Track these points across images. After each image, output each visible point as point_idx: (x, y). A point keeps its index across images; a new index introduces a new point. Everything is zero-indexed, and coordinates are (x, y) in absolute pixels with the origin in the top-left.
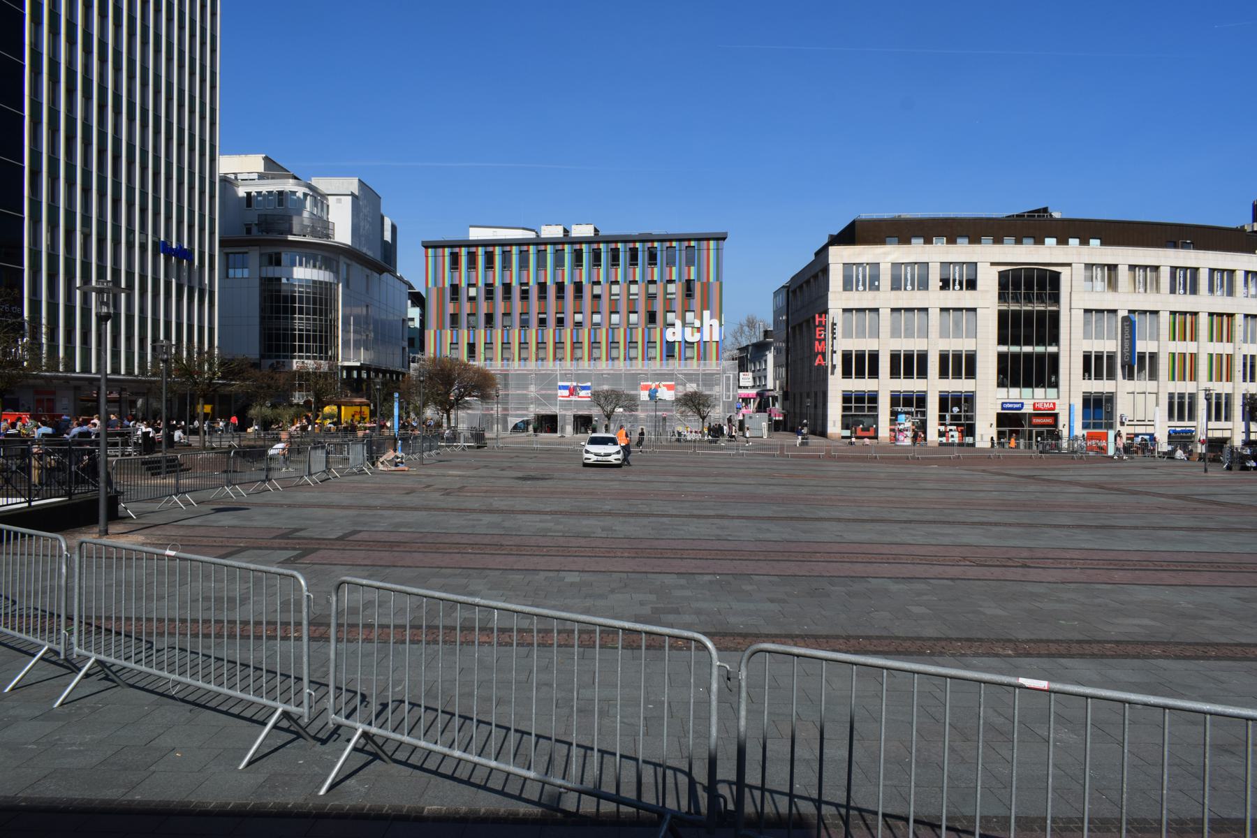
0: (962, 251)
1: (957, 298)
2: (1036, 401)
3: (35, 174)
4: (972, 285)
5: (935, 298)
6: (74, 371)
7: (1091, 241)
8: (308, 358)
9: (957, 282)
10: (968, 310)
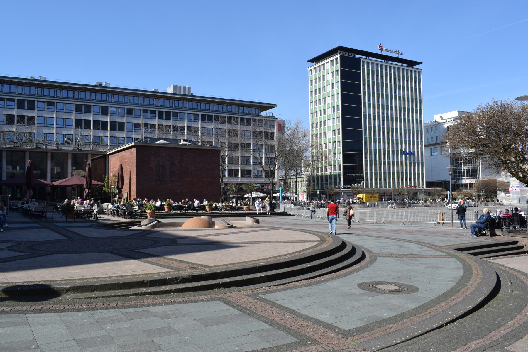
3: (366, 142)
6: (378, 188)
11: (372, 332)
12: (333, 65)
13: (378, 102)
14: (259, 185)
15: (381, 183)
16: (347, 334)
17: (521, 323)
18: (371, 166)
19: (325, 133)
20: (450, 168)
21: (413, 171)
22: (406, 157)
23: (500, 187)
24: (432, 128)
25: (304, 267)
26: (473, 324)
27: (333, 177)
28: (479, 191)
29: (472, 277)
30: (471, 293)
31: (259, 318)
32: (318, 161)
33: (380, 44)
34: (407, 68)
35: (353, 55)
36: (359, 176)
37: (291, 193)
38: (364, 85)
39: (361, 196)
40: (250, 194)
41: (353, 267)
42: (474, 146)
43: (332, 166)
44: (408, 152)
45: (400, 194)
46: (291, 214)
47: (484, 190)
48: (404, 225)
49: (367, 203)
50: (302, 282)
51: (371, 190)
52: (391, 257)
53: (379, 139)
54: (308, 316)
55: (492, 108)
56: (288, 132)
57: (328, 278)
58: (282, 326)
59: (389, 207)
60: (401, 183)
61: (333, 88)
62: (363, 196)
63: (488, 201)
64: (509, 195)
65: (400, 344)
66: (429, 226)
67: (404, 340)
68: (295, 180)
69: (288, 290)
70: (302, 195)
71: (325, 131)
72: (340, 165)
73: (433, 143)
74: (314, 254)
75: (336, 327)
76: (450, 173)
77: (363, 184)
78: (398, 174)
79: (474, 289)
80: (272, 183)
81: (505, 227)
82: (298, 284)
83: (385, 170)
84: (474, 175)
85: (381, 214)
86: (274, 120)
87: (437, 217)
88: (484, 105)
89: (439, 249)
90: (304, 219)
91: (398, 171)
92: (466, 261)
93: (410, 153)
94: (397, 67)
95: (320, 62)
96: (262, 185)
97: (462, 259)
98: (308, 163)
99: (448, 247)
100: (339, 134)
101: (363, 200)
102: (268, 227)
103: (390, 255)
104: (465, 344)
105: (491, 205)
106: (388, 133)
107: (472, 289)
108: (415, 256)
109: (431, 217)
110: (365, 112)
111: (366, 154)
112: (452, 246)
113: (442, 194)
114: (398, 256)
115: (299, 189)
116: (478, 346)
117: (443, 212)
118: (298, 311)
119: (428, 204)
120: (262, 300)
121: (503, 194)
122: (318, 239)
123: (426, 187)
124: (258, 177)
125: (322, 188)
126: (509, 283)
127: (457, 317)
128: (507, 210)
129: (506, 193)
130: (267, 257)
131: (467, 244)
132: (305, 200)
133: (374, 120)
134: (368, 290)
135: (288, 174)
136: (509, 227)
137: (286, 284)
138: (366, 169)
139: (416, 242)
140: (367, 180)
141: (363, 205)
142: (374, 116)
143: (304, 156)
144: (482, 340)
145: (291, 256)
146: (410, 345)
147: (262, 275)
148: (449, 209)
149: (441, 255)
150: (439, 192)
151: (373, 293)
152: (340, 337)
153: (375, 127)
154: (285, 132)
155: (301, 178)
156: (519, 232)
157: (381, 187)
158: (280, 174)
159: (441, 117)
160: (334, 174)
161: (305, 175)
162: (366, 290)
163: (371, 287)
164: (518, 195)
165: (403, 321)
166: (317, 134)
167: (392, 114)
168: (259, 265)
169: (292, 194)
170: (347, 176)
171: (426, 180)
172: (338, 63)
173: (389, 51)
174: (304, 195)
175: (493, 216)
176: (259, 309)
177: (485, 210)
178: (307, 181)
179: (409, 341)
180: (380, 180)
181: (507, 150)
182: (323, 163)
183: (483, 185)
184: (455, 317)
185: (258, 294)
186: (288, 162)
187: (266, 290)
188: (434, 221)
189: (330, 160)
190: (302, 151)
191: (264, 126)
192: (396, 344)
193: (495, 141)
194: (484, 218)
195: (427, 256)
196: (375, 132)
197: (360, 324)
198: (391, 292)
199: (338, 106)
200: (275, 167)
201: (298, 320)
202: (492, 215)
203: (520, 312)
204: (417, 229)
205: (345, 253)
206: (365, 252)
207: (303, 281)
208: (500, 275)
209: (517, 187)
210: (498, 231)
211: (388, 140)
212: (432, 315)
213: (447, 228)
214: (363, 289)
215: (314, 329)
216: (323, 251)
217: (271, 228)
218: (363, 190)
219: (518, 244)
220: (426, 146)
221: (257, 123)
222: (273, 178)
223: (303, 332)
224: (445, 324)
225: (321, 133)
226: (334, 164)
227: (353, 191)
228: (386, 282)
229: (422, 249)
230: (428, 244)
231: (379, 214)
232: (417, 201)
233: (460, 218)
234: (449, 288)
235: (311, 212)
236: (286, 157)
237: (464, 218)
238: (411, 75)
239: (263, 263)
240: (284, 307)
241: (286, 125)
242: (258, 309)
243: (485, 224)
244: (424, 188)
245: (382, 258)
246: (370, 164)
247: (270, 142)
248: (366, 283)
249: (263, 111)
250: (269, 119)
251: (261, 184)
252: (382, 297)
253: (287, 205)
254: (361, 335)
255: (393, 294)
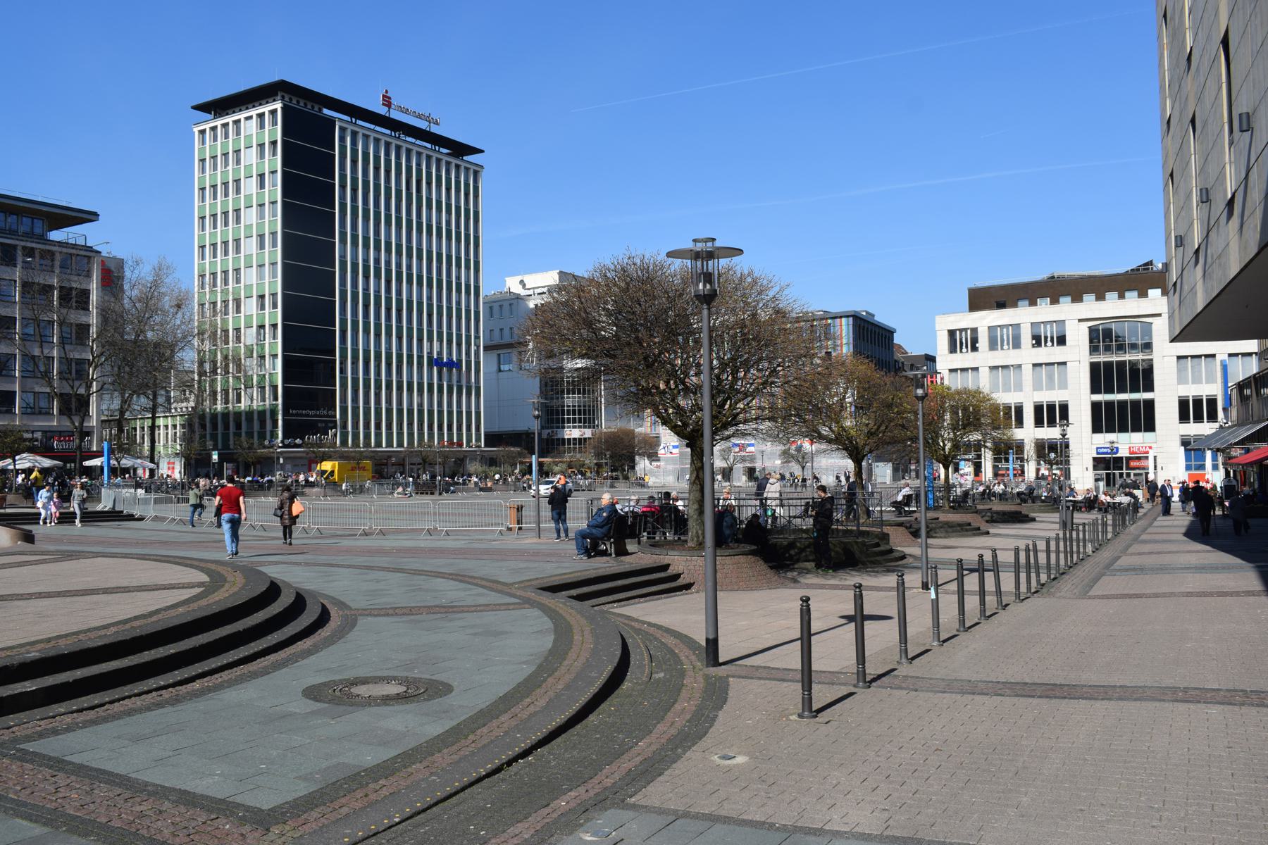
0: (1045, 311)
1: (1049, 353)
2: (1132, 445)
3: (343, 332)
4: (1062, 341)
5: (1028, 355)
6: (371, 447)
7: (1150, 292)
8: (574, 427)
9: (1049, 339)
10: (1059, 364)
11: (332, 805)
12: (262, 126)
13: (377, 233)
14: (38, 435)
15: (378, 435)
16: (263, 820)
17: (662, 741)
18: (355, 391)
19: (238, 302)
20: (536, 401)
21: (457, 407)
22: (440, 373)
23: (640, 448)
24: (501, 306)
25: (159, 656)
26: (567, 755)
27: (256, 417)
28: (599, 455)
29: (572, 650)
30: (568, 687)
31: (12, 809)
32: (217, 374)
33: (387, 92)
34: (449, 159)
35: (316, 109)
36: (324, 416)
37: (138, 458)
38: (343, 187)
39: (327, 466)
40: (9, 461)
41: (294, 646)
42: (586, 354)
43: (255, 389)
44: (445, 360)
45: (424, 461)
46: (133, 515)
47: (608, 453)
48: (384, 537)
49: (344, 485)
50: (150, 696)
51: (355, 452)
52: (392, 615)
53: (378, 326)
54: (164, 787)
55: (625, 271)
56: (131, 291)
57: (226, 679)
58: (83, 821)
59: (398, 493)
60: (429, 434)
61: (262, 186)
62: (334, 466)
63: (617, 478)
64: (658, 464)
65: (400, 826)
66: (486, 537)
67: (409, 815)
68: (148, 423)
69: (108, 722)
70: (169, 463)
71: (236, 297)
72: (275, 388)
73: (502, 342)
74: (189, 619)
75: (238, 805)
76: (537, 413)
77: (334, 436)
78: (421, 412)
79: (572, 676)
80: (82, 429)
81: (645, 534)
82: (138, 702)
83: (389, 401)
84: (590, 419)
85: (376, 512)
86: (89, 257)
87: (506, 516)
88: (608, 263)
89: (506, 589)
90: (173, 527)
91: (420, 405)
92: (561, 615)
93: (450, 364)
94: (425, 152)
95: (227, 114)
96: (49, 434)
97: (554, 611)
98: (186, 378)
99: (524, 585)
100: (275, 306)
101: (332, 476)
102: (58, 551)
103: (391, 612)
104: (545, 803)
105: (621, 486)
106: (399, 311)
107: (568, 677)
108: (451, 610)
109: (492, 515)
110: (343, 257)
111: (343, 362)
112: (533, 583)
113: (521, 463)
114: (410, 611)
115: (160, 447)
116: (573, 804)
117: (520, 504)
118: (134, 776)
119: (489, 484)
120: (26, 757)
121: (647, 461)
122: (204, 578)
123: (486, 445)
124: (37, 411)
125: (226, 445)
126: (646, 657)
127: (534, 743)
128: (652, 497)
129: (653, 460)
130: (50, 636)
131: (566, 576)
132: (177, 476)
133: (366, 277)
134: (329, 702)
135: (129, 405)
136: (654, 533)
137: (103, 705)
138: (344, 399)
139: (454, 577)
140: (344, 426)
141: (333, 489)
142: (366, 268)
143: (176, 358)
144: (582, 789)
145: (121, 627)
146: (423, 823)
147: (30, 686)
148: (534, 497)
149: (509, 604)
150: (514, 457)
151: (342, 708)
152: (247, 828)
153: (366, 296)
154: (122, 290)
155: (166, 417)
156: (670, 545)
157: (379, 444)
158: (104, 407)
159: (522, 282)
160: (260, 408)
161: (179, 410)
162: (324, 702)
163: (337, 693)
164: (674, 464)
165: (409, 770)
166: (214, 304)
167: (409, 267)
168: (22, 661)
169: (139, 461)
170: (293, 415)
171: (485, 428)
172: (276, 125)
173: (406, 111)
174: (174, 463)
175: (622, 510)
176: (14, 785)
177: (606, 498)
178: (183, 426)
179: (422, 815)
180: (378, 426)
181: (651, 364)
182: (231, 378)
183: (606, 441)
184: (530, 745)
185: (16, 740)
186: (131, 374)
187: (39, 729)
188: (499, 524)
189: (250, 373)
190: (172, 347)
191: (57, 271)
192: (390, 827)
193: (629, 344)
194: (605, 514)
195: (477, 608)
196: (366, 307)
197: (302, 789)
198: (388, 702)
199: (274, 234)
200: (89, 386)
201: (131, 801)
202: (621, 507)
203: (663, 717)
204: (459, 544)
205: (275, 612)
206: (329, 606)
207: (154, 694)
208: (629, 641)
209: (674, 447)
210: (632, 543)
211: (399, 329)
212: (479, 746)
213: (527, 541)
214: (316, 699)
215: (178, 819)
216: (216, 609)
217: (69, 556)
218: (335, 452)
219: (669, 571)
220: (486, 348)
221: (37, 259)
222: (85, 415)
223: (144, 832)
224: (506, 763)
225: (225, 301)
226: (259, 383)
227: (307, 453)
228: (375, 678)
229: (467, 593)
230: (482, 579)
231: (370, 512)
232: (465, 477)
233: (556, 516)
234: (521, 679)
235: (192, 509)
236: (124, 358)
237: (563, 517)
238: (457, 177)
239: (33, 654)
240: (91, 769)
241: (128, 273)
242: (11, 783)
243: (606, 528)
244: (480, 447)
245: (370, 618)
246: (352, 387)
247: (75, 317)
248: (325, 684)
249: (57, 229)
250: (74, 251)
251: (46, 432)
252: (362, 717)
253: (124, 491)
254: (305, 816)
255: (393, 705)
